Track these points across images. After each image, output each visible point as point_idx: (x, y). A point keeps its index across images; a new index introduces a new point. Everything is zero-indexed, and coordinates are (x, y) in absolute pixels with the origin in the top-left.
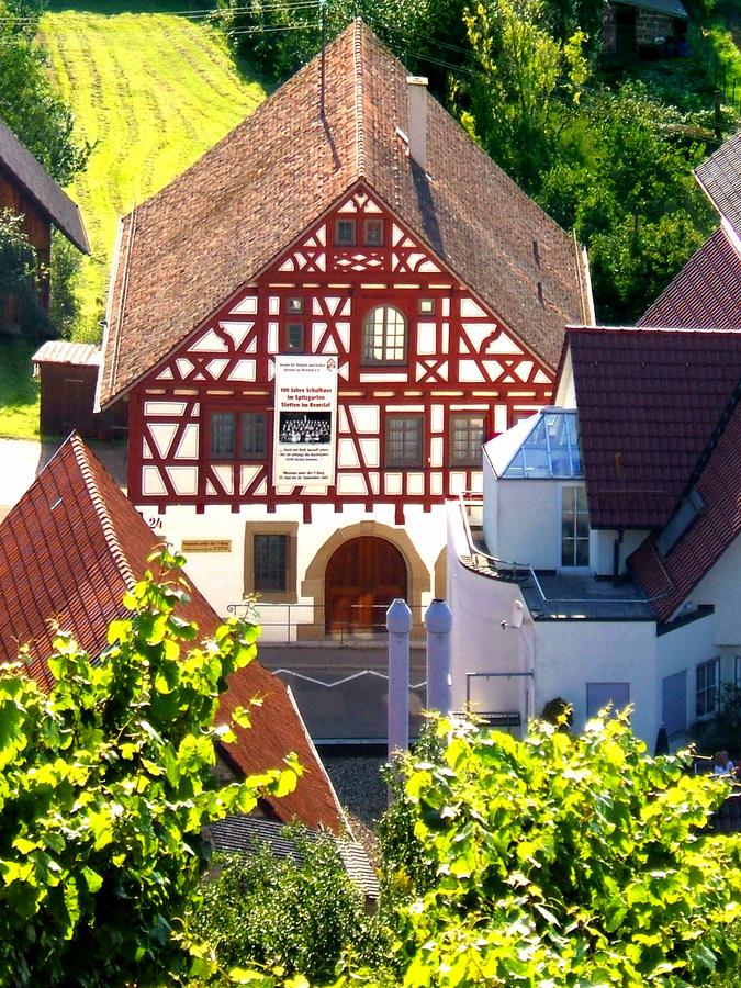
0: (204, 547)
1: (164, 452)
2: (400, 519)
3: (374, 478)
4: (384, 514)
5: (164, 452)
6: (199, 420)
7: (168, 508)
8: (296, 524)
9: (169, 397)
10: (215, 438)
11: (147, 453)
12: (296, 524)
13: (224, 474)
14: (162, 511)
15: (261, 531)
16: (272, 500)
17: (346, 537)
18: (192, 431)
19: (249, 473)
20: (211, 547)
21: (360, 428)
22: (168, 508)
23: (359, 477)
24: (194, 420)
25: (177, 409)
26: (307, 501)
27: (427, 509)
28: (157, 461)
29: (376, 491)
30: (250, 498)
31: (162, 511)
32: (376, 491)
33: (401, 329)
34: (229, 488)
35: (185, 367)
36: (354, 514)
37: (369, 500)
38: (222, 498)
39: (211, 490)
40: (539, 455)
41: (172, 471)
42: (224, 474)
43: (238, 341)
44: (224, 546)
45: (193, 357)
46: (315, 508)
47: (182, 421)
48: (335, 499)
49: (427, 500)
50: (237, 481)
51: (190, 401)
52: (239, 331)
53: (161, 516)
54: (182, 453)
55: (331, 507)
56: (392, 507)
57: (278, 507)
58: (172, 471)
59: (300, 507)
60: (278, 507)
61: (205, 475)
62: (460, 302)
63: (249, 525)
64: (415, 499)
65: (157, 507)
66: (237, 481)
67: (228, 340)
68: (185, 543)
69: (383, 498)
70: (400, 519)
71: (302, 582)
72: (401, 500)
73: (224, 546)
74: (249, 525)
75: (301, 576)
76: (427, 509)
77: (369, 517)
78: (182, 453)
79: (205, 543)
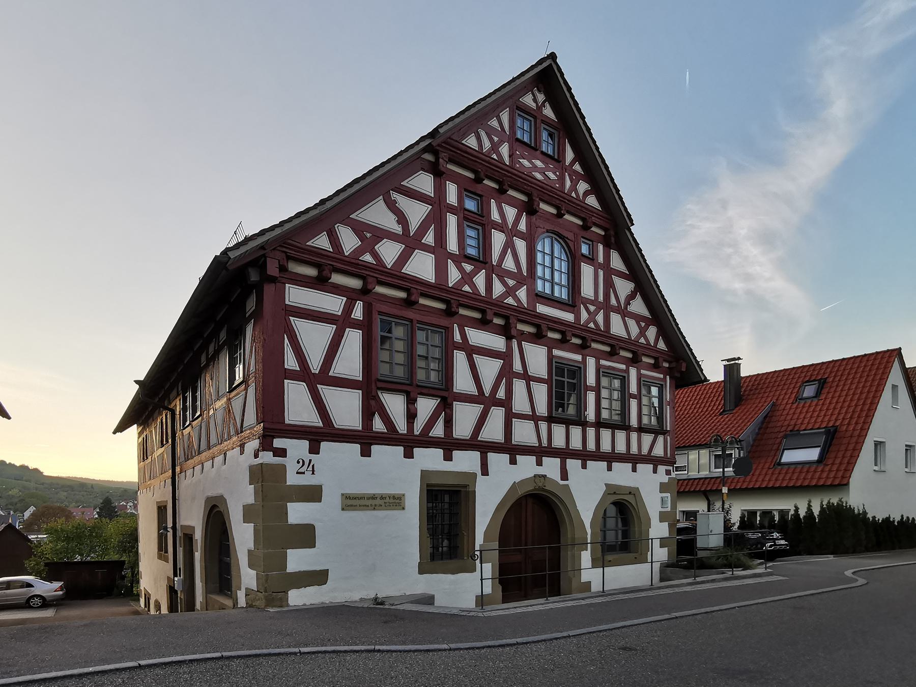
0: (369, 502)
1: (315, 364)
2: (564, 475)
3: (591, 432)
4: (551, 467)
5: (315, 364)
6: (366, 326)
7: (324, 445)
8: (474, 475)
9: (321, 283)
10: (261, 384)
11: (291, 362)
12: (474, 475)
13: (395, 404)
14: (314, 450)
15: (434, 481)
16: (449, 445)
17: (521, 492)
18: (353, 339)
19: (426, 406)
20: (382, 502)
21: (532, 371)
22: (324, 445)
23: (530, 425)
24: (355, 325)
25: (333, 304)
26: (485, 448)
27: (366, 453)
28: (304, 374)
29: (545, 443)
30: (426, 441)
31: (314, 450)
32: (545, 443)
33: (564, 266)
34: (401, 426)
35: (349, 241)
36: (527, 467)
37: (540, 452)
38: (391, 438)
39: (378, 425)
40: (156, 482)
41: (328, 393)
42: (395, 404)
43: (414, 226)
44: (396, 502)
45: (359, 229)
46: (492, 456)
47: (342, 322)
48: (512, 450)
49: (584, 456)
50: (411, 416)
51: (352, 296)
52: (417, 212)
53: (313, 456)
54: (339, 369)
55: (506, 457)
56: (557, 461)
57: (456, 454)
58: (328, 393)
59: (476, 455)
60: (456, 454)
61: (371, 407)
62: (445, 304)
63: (425, 474)
64: (575, 454)
65: (744, 373)
66: (411, 416)
67: (402, 219)
68: (875, 466)
69: (552, 452)
70: (564, 475)
71: (649, 551)
72: (565, 454)
73: (396, 502)
74: (425, 474)
75: (479, 539)
76: (366, 453)
77: (540, 471)
78: (339, 369)
79: (373, 497)
